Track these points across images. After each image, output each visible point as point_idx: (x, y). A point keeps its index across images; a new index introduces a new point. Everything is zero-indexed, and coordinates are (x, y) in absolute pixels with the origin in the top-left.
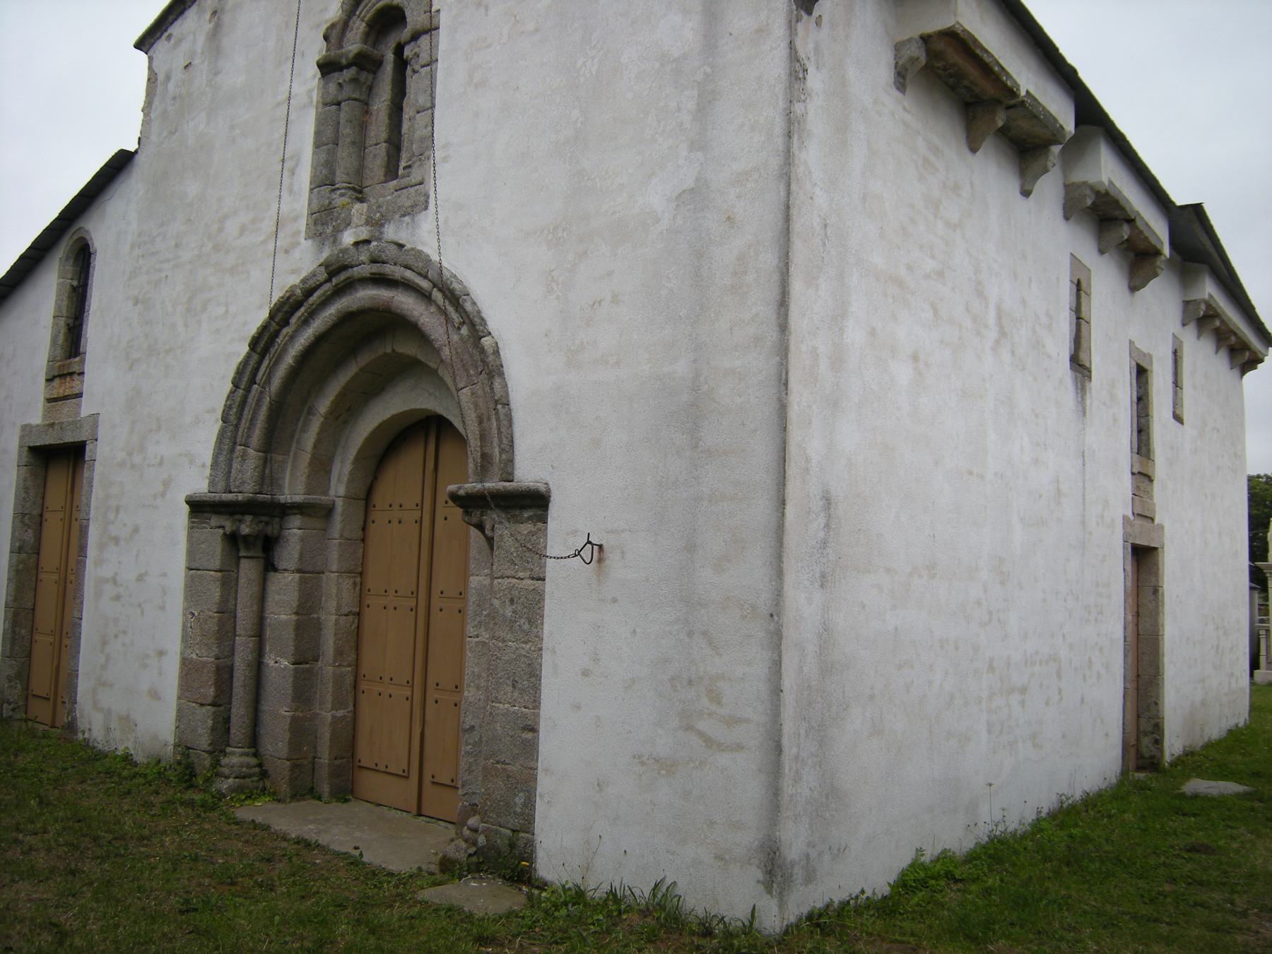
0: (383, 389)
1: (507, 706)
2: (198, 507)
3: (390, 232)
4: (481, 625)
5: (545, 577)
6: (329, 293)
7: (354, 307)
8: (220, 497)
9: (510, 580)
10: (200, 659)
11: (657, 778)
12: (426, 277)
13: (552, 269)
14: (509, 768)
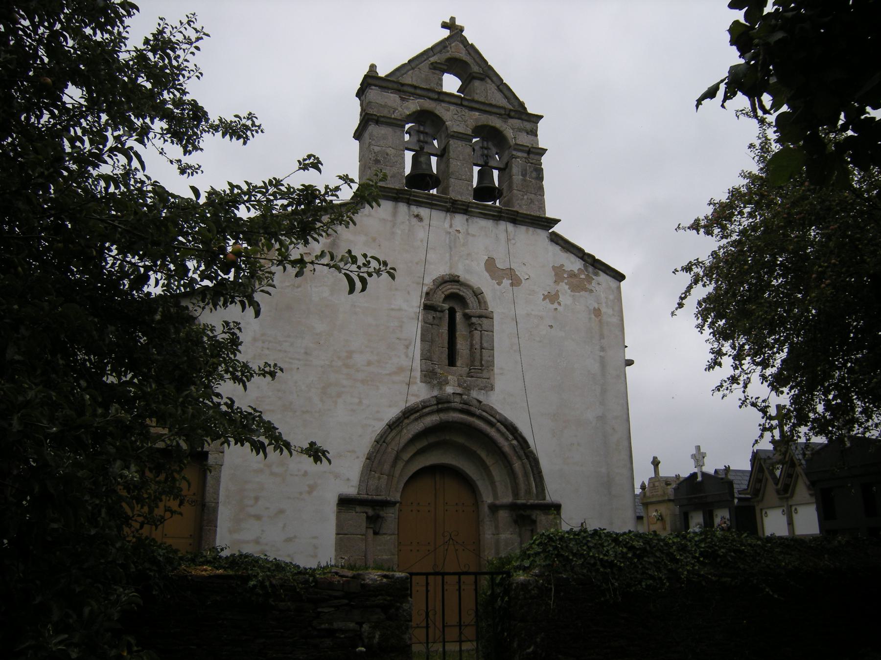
2: (345, 503)
3: (474, 394)
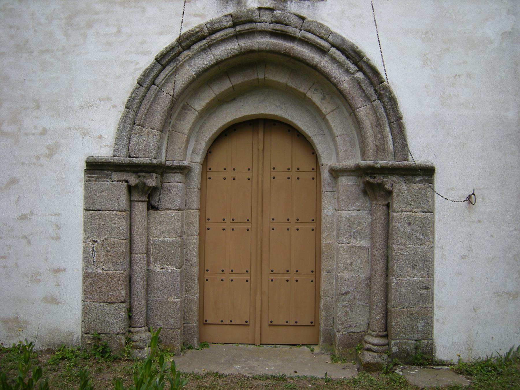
0: (234, 99)
1: (409, 278)
4: (351, 237)
6: (231, 35)
7: (256, 47)
8: (124, 160)
9: (407, 213)
10: (106, 272)
11: (508, 301)
12: (326, 40)
13: (426, 53)
14: (412, 309)
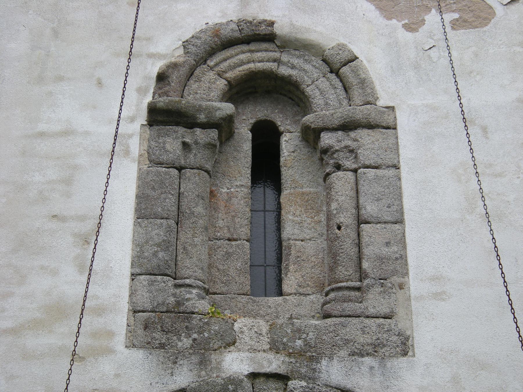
5: (396, 125)
